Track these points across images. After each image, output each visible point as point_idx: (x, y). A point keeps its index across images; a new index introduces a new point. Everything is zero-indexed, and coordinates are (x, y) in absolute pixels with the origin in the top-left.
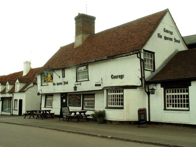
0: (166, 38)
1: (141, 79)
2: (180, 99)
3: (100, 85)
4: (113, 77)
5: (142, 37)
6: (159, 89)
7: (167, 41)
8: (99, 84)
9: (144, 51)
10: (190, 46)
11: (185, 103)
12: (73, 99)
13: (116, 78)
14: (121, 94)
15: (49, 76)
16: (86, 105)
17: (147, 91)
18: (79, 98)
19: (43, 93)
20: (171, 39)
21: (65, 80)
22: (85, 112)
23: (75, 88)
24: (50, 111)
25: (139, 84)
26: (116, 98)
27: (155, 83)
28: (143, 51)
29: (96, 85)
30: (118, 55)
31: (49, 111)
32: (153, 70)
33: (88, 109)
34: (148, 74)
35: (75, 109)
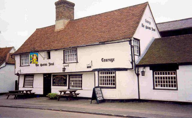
0: (147, 28)
1: (132, 63)
2: (108, 79)
3: (90, 67)
4: (103, 60)
5: (129, 26)
6: (149, 72)
7: (148, 30)
8: (89, 66)
9: (134, 39)
10: (164, 34)
11: (173, 84)
12: (58, 79)
13: (107, 61)
14: (113, 75)
15: (35, 57)
16: (73, 85)
17: (137, 73)
18: (65, 78)
19: (23, 73)
20: (150, 28)
21: (51, 61)
22: (75, 91)
23: (64, 69)
24: (31, 91)
25: (131, 67)
26: (104, 79)
27: (144, 66)
29: (88, 67)
30: (108, 41)
31: (30, 91)
32: (138, 54)
33: (77, 88)
34: (137, 59)
35: (55, 90)
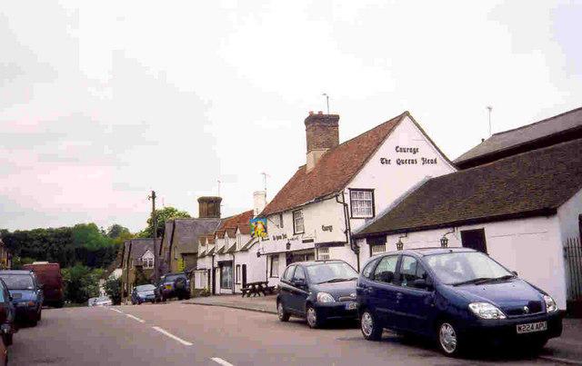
0: (399, 162)
3: (312, 241)
15: (260, 226)
20: (413, 162)
28: (346, 191)
